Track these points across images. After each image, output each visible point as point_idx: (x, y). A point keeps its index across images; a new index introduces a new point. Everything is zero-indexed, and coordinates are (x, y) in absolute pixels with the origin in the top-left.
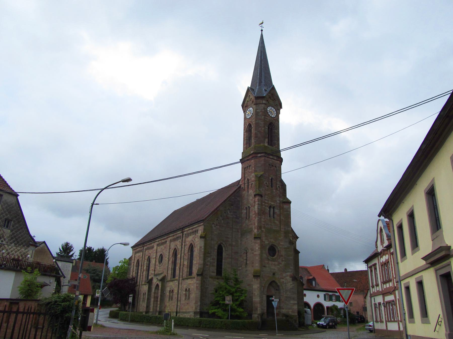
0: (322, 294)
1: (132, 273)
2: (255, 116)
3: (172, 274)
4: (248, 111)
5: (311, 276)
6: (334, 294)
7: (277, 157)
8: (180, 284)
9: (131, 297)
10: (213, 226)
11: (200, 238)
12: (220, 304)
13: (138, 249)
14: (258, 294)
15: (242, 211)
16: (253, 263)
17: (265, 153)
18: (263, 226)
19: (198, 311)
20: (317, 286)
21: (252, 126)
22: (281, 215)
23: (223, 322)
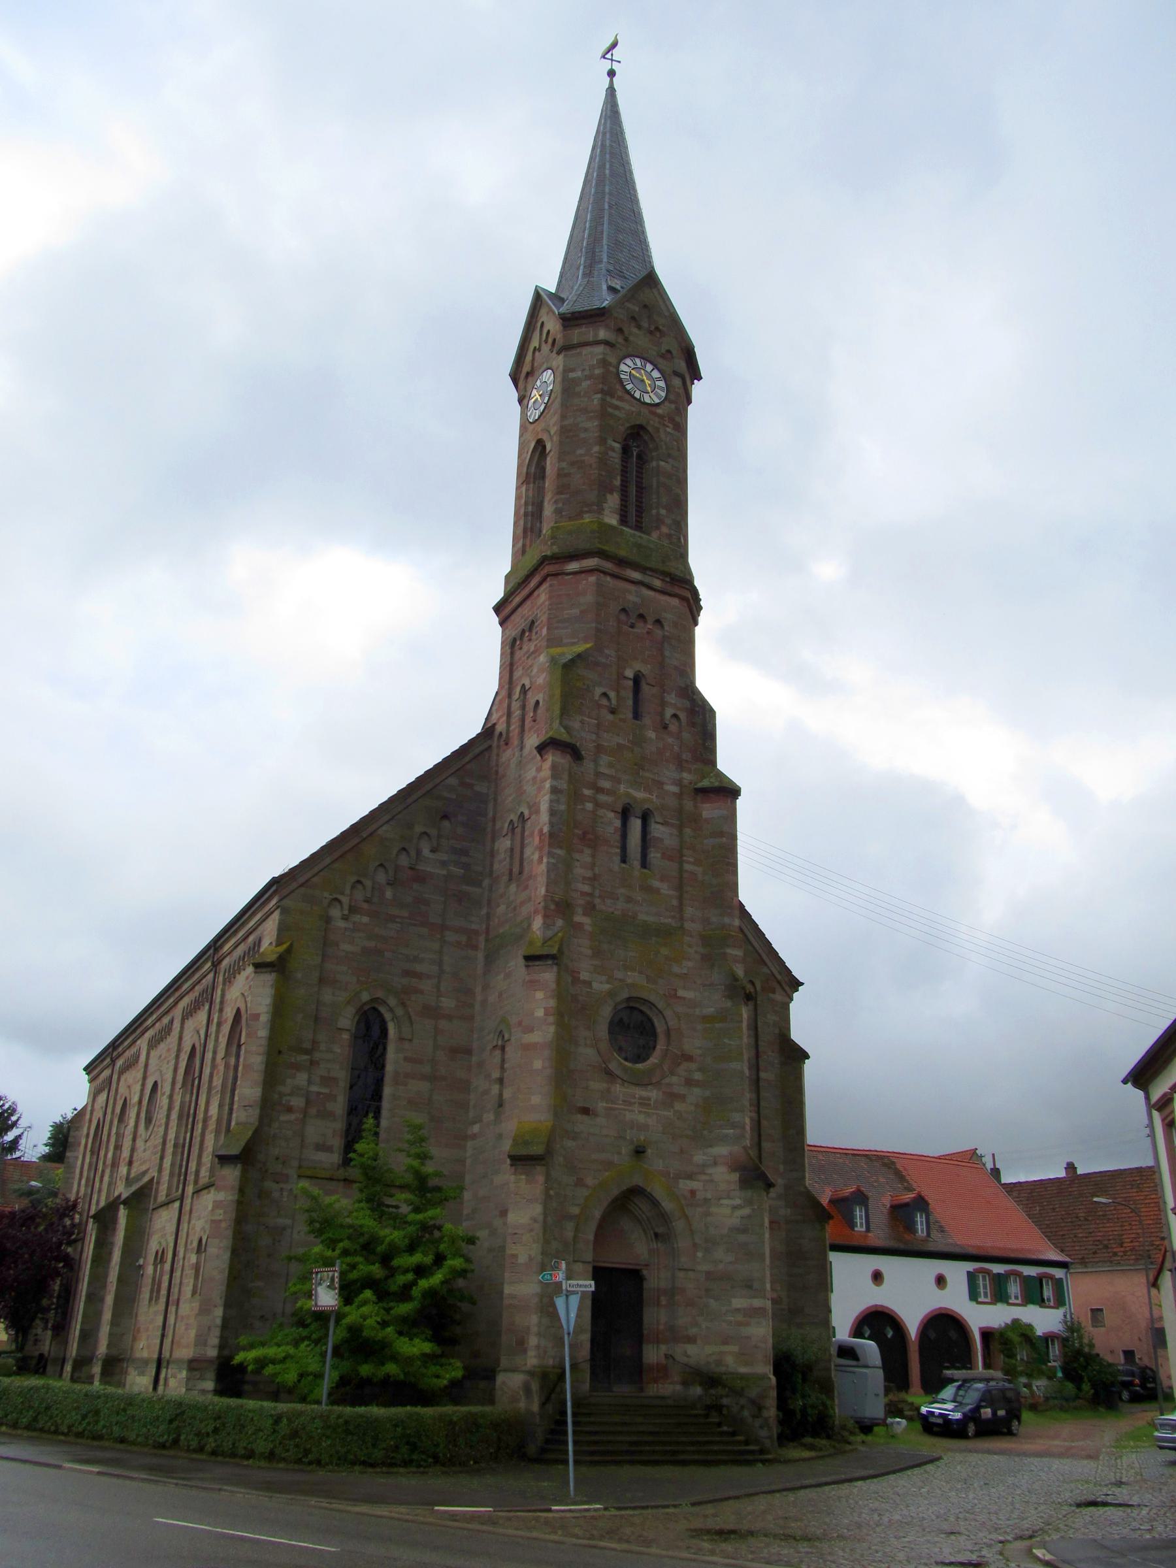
0: (957, 1272)
2: (559, 400)
5: (909, 1189)
6: (1012, 1270)
10: (335, 912)
14: (531, 1259)
15: (497, 844)
18: (581, 902)
19: (212, 1353)
20: (935, 1234)
21: (548, 447)
22: (685, 852)
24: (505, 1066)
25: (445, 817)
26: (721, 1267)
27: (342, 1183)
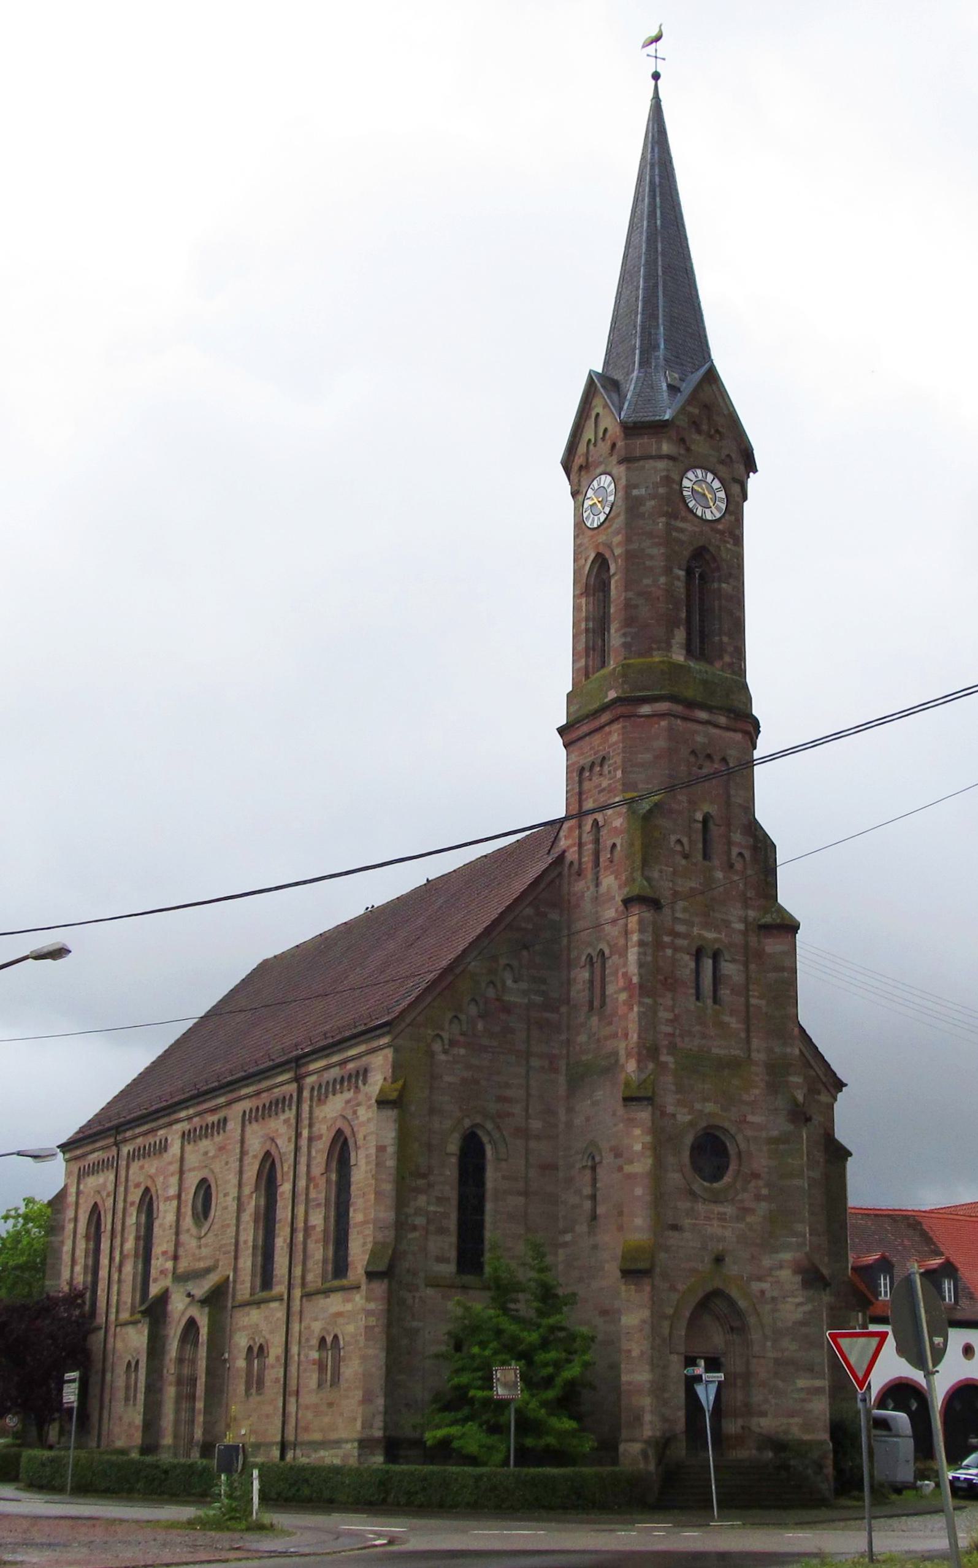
1: (69, 1268)
3: (259, 1270)
4: (590, 493)
5: (937, 1253)
7: (732, 715)
8: (295, 1318)
9: (73, 1381)
10: (437, 1047)
11: (378, 1108)
12: (471, 1401)
13: (96, 1155)
14: (642, 1353)
16: (622, 1212)
17: (673, 698)
19: (379, 1434)
20: (964, 1303)
21: (612, 570)
22: (751, 987)
23: (485, 1479)
25: (526, 947)
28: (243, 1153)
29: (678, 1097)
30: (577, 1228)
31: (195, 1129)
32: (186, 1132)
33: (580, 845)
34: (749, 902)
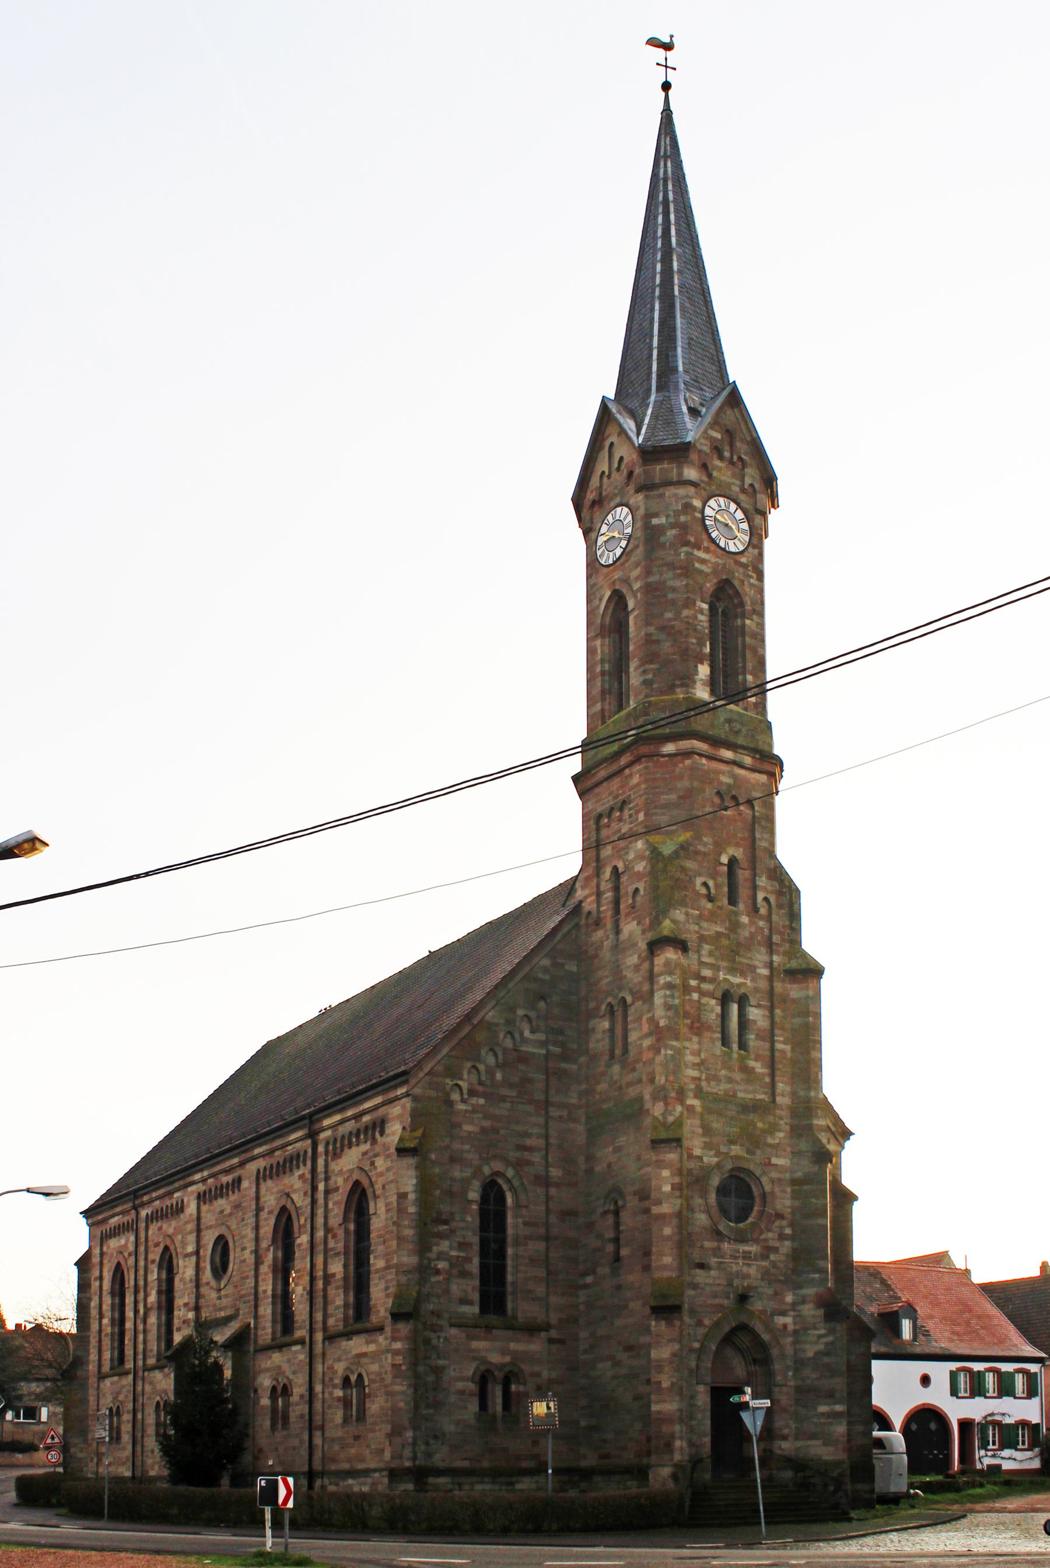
0: (940, 1371)
1: (97, 1322)
7: (758, 756)
10: (455, 1096)
11: (398, 1156)
13: (116, 1219)
22: (777, 1032)
24: (621, 1228)
25: (542, 998)
26: (809, 1382)
27: (483, 1330)
28: (259, 1209)
29: (705, 1139)
30: (599, 1270)
31: (210, 1190)
32: (202, 1193)
33: (599, 894)
34: (774, 947)
